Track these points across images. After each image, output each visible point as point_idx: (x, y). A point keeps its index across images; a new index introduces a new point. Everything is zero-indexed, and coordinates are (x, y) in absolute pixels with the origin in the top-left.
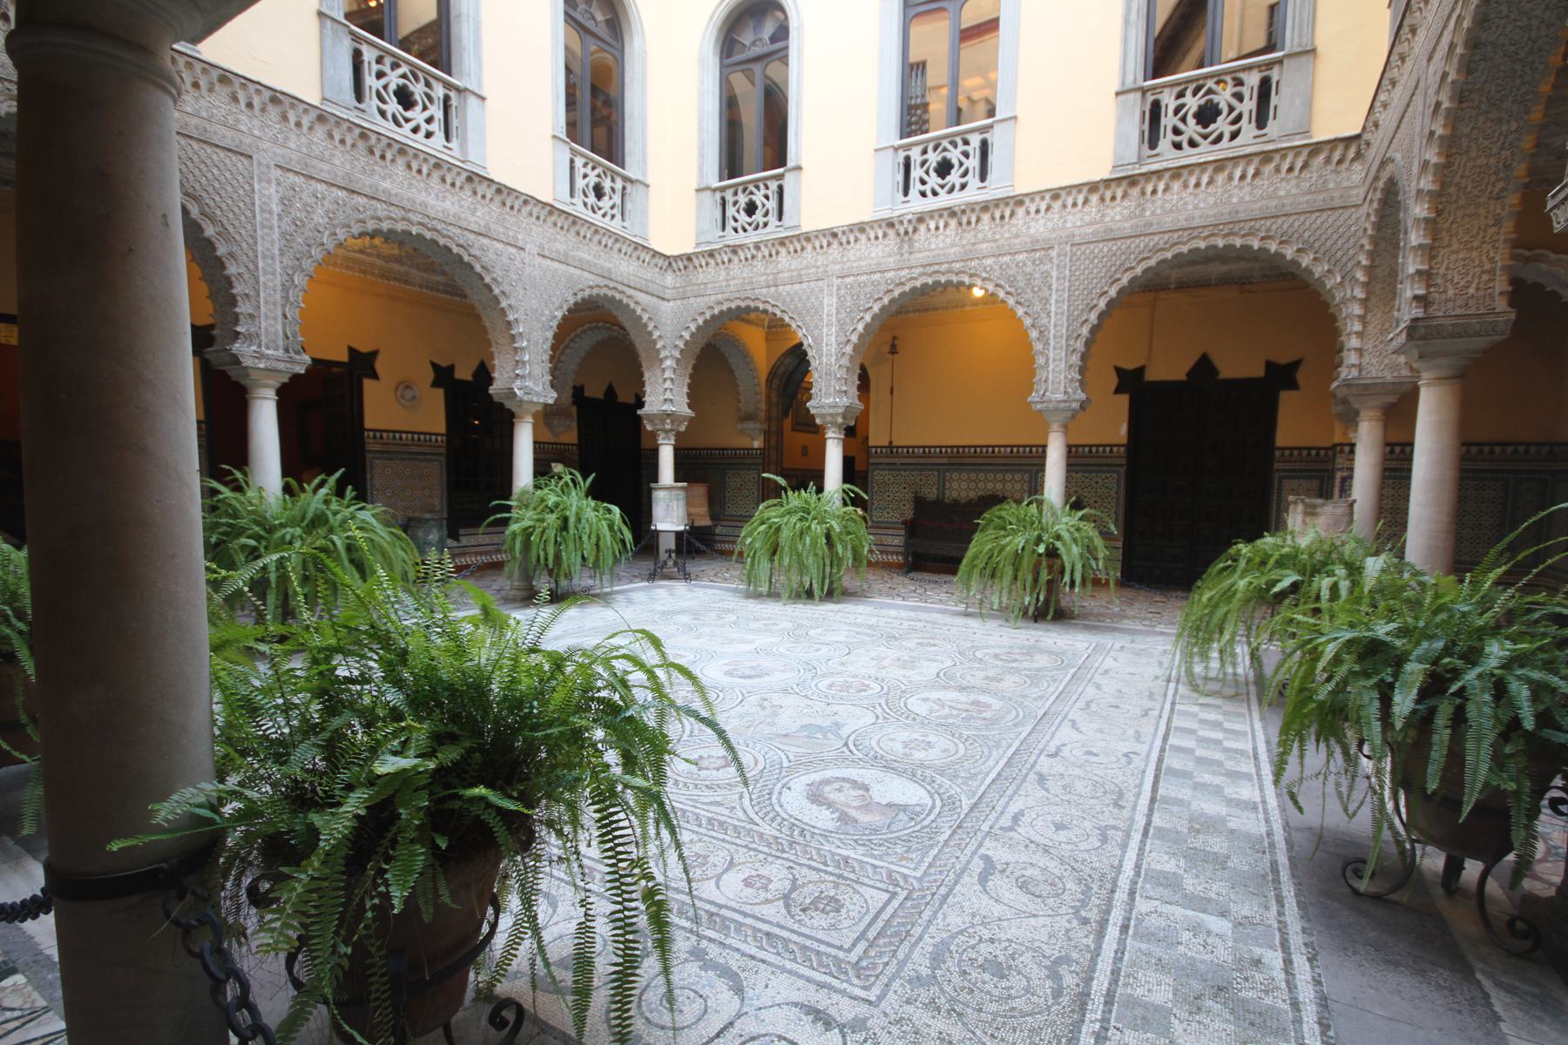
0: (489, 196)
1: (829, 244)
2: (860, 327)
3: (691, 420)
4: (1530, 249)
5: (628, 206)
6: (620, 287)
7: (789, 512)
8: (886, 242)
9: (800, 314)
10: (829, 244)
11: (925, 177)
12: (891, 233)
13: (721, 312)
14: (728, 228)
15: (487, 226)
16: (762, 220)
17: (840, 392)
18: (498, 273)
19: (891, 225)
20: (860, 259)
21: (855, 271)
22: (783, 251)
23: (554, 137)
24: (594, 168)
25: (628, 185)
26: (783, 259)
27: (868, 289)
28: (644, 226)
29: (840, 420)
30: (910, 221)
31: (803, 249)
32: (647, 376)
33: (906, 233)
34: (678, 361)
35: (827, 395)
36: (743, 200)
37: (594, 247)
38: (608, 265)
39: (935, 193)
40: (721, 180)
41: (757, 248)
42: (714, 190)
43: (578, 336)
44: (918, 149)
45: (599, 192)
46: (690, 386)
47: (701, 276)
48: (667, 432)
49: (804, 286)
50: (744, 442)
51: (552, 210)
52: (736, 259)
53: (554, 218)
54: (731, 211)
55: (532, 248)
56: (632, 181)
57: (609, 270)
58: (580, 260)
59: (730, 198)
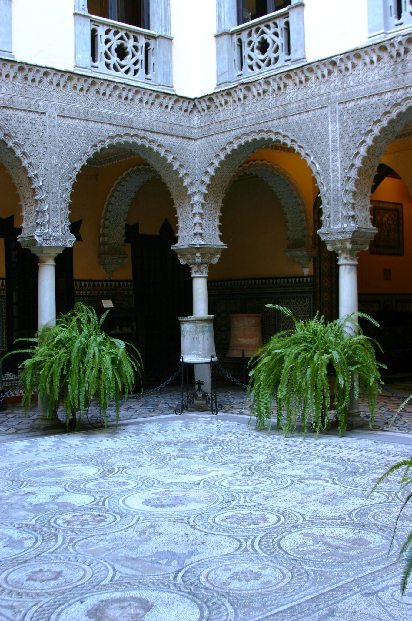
0: (12, 75)
1: (330, 73)
2: (363, 151)
3: (224, 252)
4: (113, 186)
5: (152, 59)
6: (142, 134)
7: (296, 343)
8: (381, 65)
9: (308, 142)
10: (330, 73)
11: (275, 38)
12: (385, 56)
13: (240, 146)
14: (245, 66)
15: (11, 100)
16: (273, 56)
17: (347, 217)
18: (20, 138)
19: (383, 48)
20: (359, 84)
21: (355, 96)
22: (290, 83)
23: (75, 14)
24: (116, 33)
25: (152, 42)
26: (292, 92)
27: (367, 113)
28: (168, 74)
29: (349, 246)
30: (400, 43)
31: (307, 79)
32: (179, 212)
33: (398, 55)
34: (205, 196)
35: (336, 221)
36: (256, 39)
37: (114, 100)
38: (128, 115)
39: (260, 67)
40: (238, 24)
41: (268, 83)
42: (232, 34)
43: (124, 179)
44: (247, 32)
45: (121, 52)
46: (221, 219)
47: (222, 114)
48: (199, 265)
49: (311, 114)
50: (295, 270)
51: (70, 75)
52: (250, 95)
53: (74, 82)
54: (247, 51)
55: (52, 111)
56: (155, 38)
57: (130, 120)
58: (100, 115)
59: (245, 38)
